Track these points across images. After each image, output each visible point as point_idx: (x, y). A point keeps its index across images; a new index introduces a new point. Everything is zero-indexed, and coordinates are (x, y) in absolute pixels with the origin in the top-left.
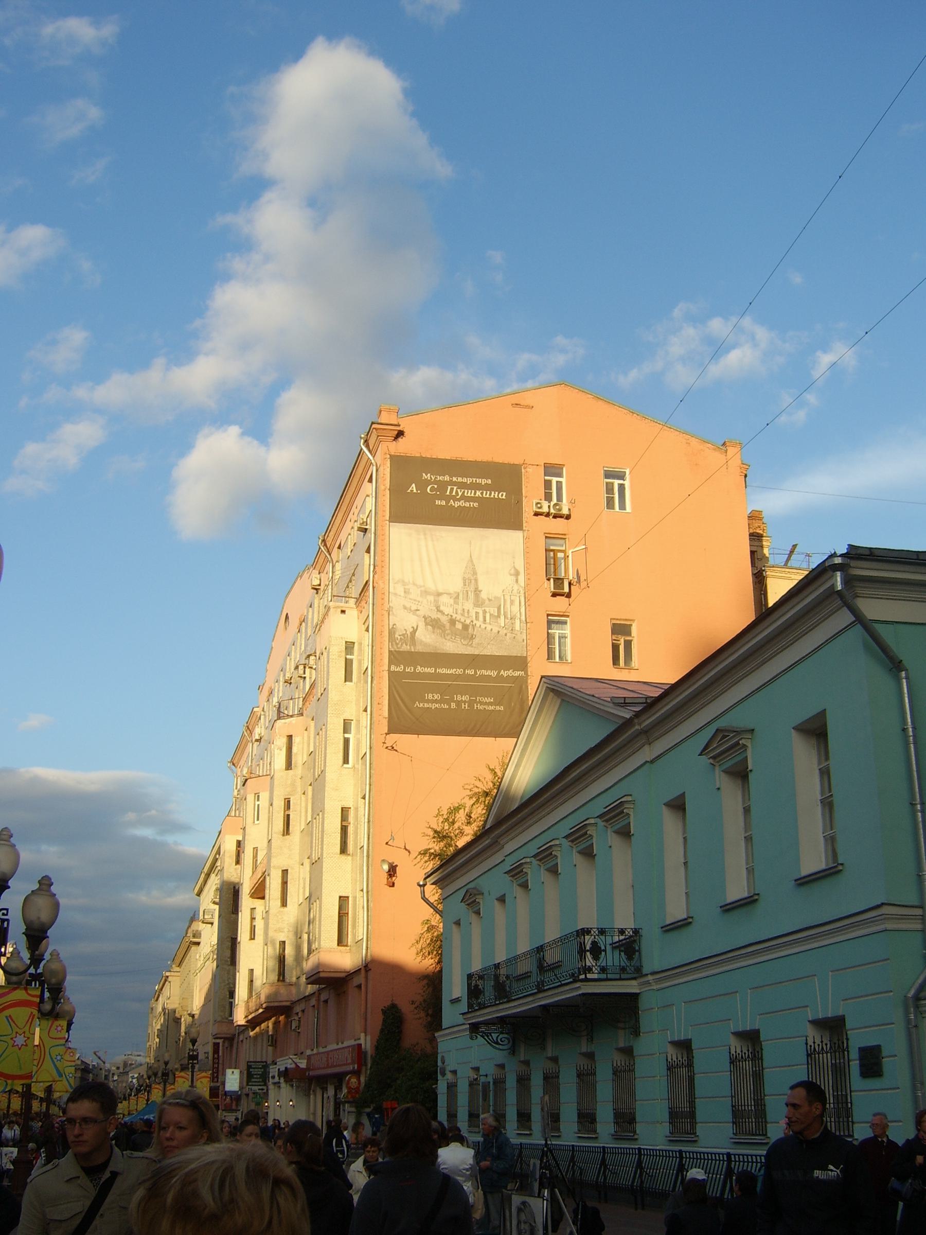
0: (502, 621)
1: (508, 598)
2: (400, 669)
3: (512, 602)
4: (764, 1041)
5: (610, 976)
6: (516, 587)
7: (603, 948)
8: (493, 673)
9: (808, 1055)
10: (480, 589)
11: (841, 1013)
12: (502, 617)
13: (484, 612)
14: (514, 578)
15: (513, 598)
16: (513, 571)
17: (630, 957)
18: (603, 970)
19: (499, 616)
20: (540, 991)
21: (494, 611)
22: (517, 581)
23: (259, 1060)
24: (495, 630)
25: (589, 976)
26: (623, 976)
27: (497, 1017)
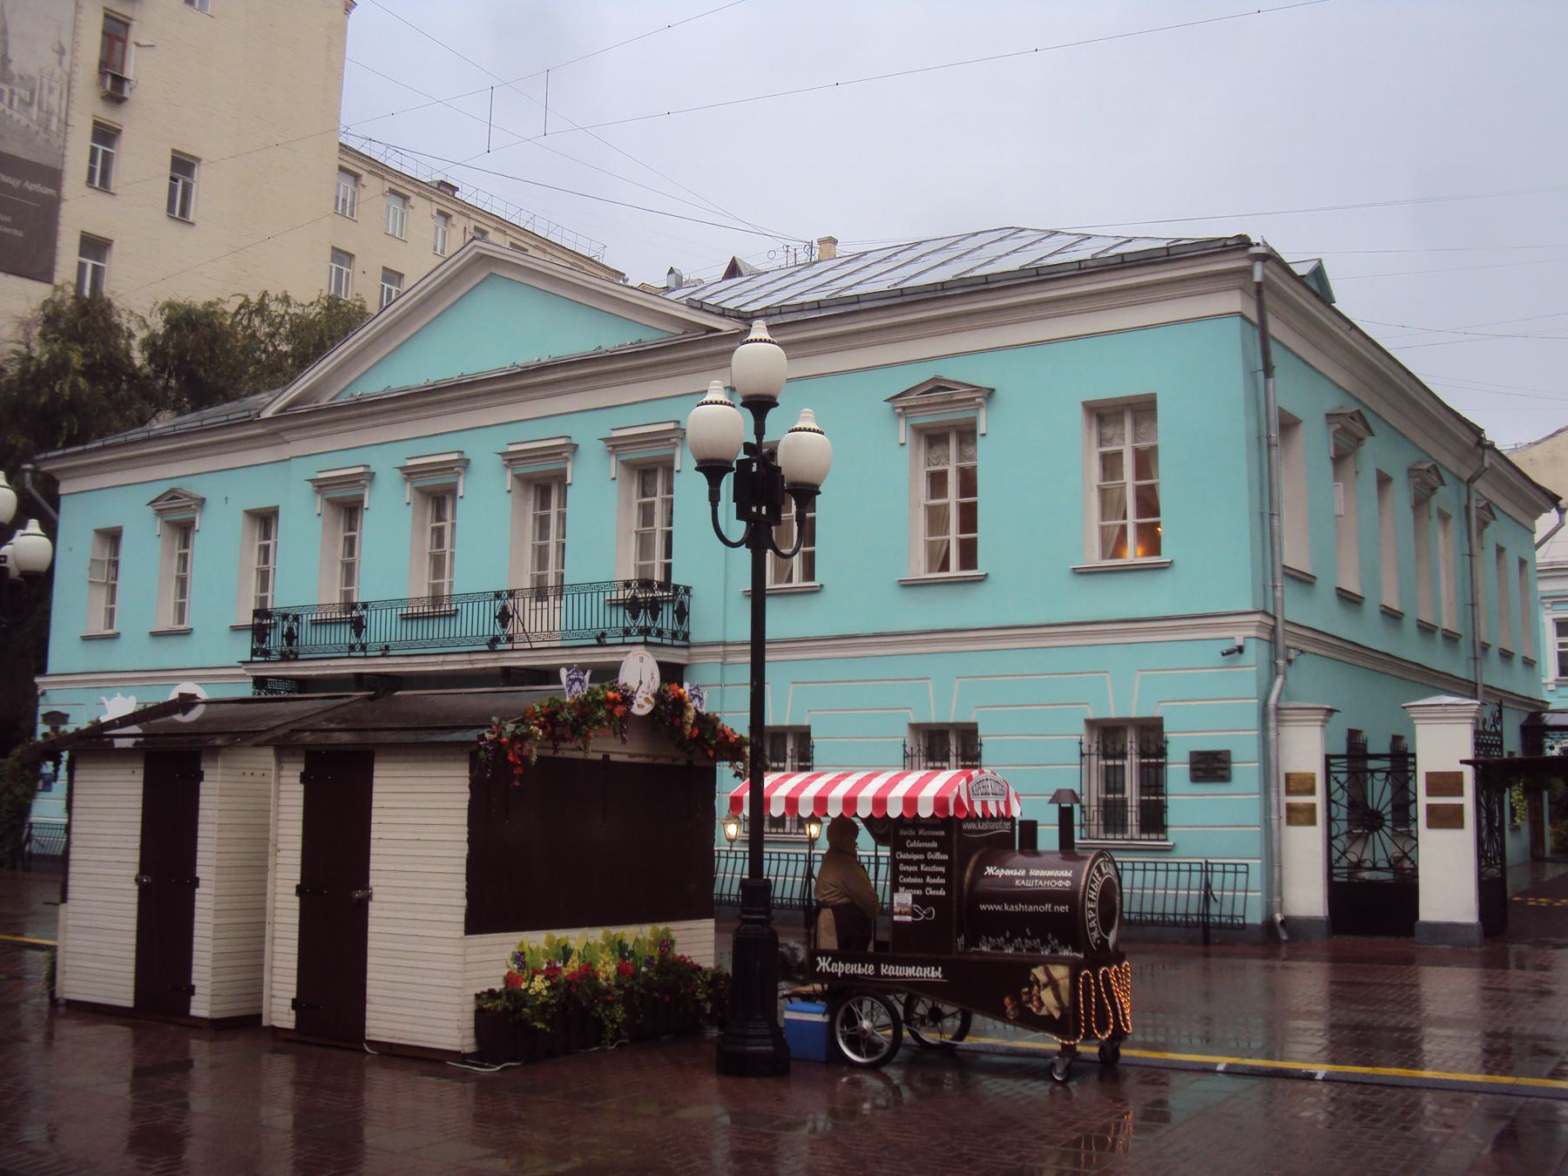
0: (34, 111)
1: (45, 81)
2: (1146, 798)
3: (51, 90)
4: (771, 642)
5: (665, 641)
6: (58, 71)
7: (497, 620)
8: (15, 183)
9: (1082, 755)
10: (10, 57)
11: (972, 720)
12: (35, 108)
13: (12, 93)
14: (56, 56)
15: (53, 84)
16: (56, 47)
17: (681, 622)
18: (660, 633)
19: (30, 104)
20: (601, 644)
21: (26, 95)
22: (61, 63)
23: (771, 632)
24: (24, 121)
25: (649, 639)
26: (352, 654)
27: (354, 674)
